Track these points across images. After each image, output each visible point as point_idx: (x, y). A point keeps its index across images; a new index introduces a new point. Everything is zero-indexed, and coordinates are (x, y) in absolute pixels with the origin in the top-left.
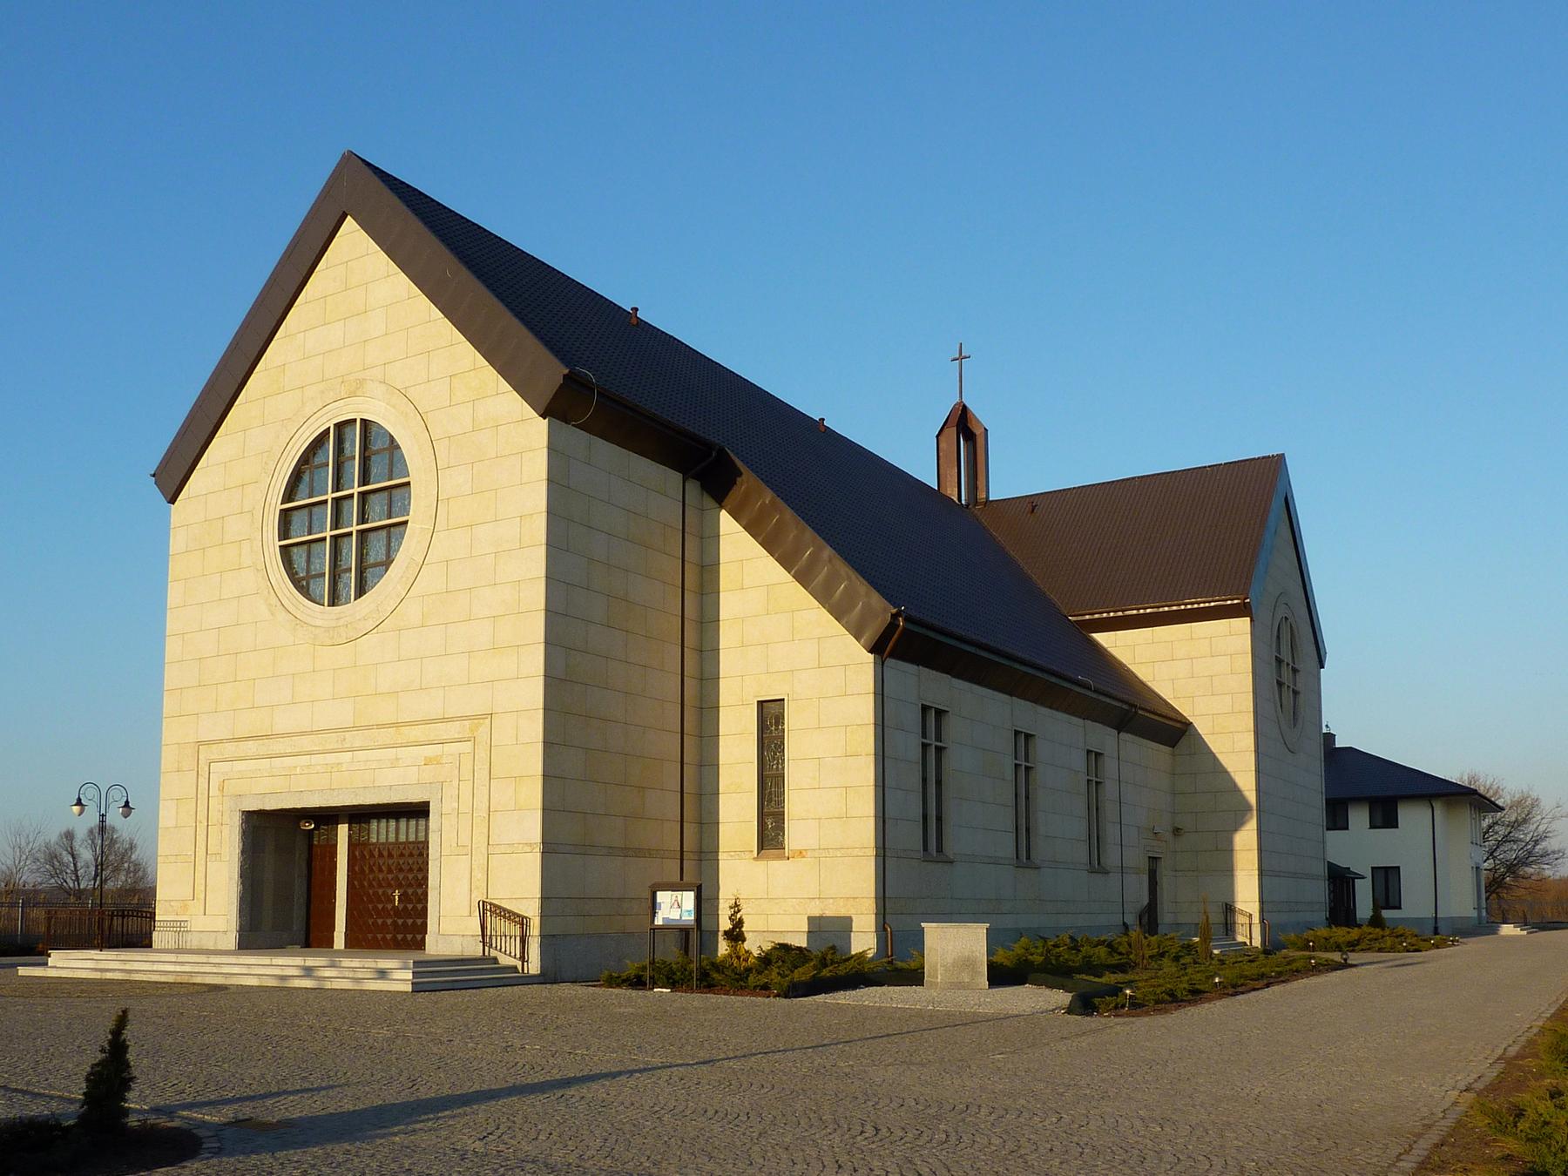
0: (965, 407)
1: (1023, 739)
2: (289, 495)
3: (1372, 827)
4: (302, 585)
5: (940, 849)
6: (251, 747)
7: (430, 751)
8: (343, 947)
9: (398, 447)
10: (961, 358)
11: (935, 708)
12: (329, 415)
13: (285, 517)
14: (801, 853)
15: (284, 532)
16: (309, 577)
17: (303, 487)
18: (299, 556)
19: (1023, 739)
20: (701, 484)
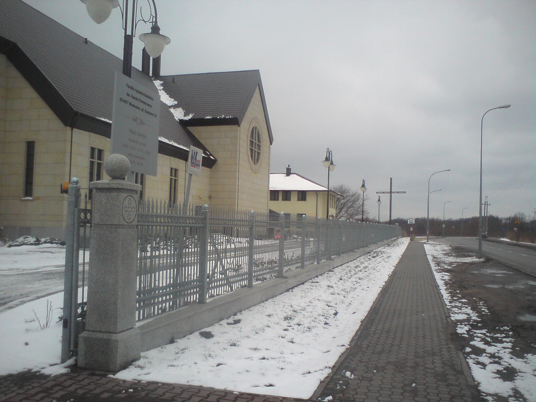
3: (298, 200)
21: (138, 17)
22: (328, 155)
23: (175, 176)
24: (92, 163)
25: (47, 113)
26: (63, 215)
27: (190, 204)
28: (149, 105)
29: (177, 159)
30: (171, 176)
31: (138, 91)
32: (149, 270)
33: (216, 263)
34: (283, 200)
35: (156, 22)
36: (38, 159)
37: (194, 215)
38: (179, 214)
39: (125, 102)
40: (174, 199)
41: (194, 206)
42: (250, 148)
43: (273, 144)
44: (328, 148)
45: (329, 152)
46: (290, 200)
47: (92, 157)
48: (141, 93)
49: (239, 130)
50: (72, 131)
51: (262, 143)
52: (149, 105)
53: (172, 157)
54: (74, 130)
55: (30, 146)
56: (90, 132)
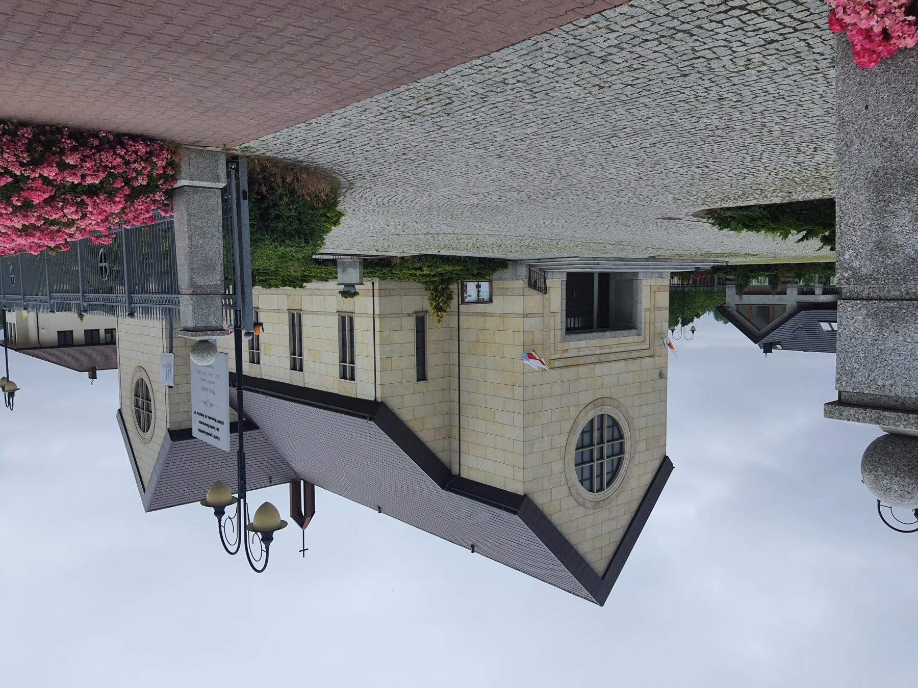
0: (302, 527)
1: (297, 365)
2: (620, 461)
3: (72, 332)
4: (615, 424)
5: (343, 319)
6: (634, 355)
7: (566, 355)
8: (833, 356)
9: (580, 481)
10: (304, 550)
11: (347, 379)
12: (606, 494)
13: (622, 452)
14: (409, 315)
15: (622, 444)
16: (612, 426)
17: (615, 464)
18: (616, 435)
19: (297, 365)
20: (451, 472)
21: (235, 520)
22: (11, 400)
23: (295, 359)
24: (352, 362)
25: (406, 415)
26: (194, 294)
28: (201, 423)
29: (253, 375)
30: (301, 360)
31: (211, 435)
34: (98, 330)
35: (220, 521)
39: (219, 422)
40: (294, 326)
42: (150, 401)
43: (117, 410)
44: (11, 410)
45: (9, 404)
46: (58, 332)
47: (353, 369)
48: (208, 434)
49: (168, 425)
50: (376, 397)
51: (134, 409)
52: (201, 423)
54: (373, 399)
55: (422, 376)
56: (305, 387)
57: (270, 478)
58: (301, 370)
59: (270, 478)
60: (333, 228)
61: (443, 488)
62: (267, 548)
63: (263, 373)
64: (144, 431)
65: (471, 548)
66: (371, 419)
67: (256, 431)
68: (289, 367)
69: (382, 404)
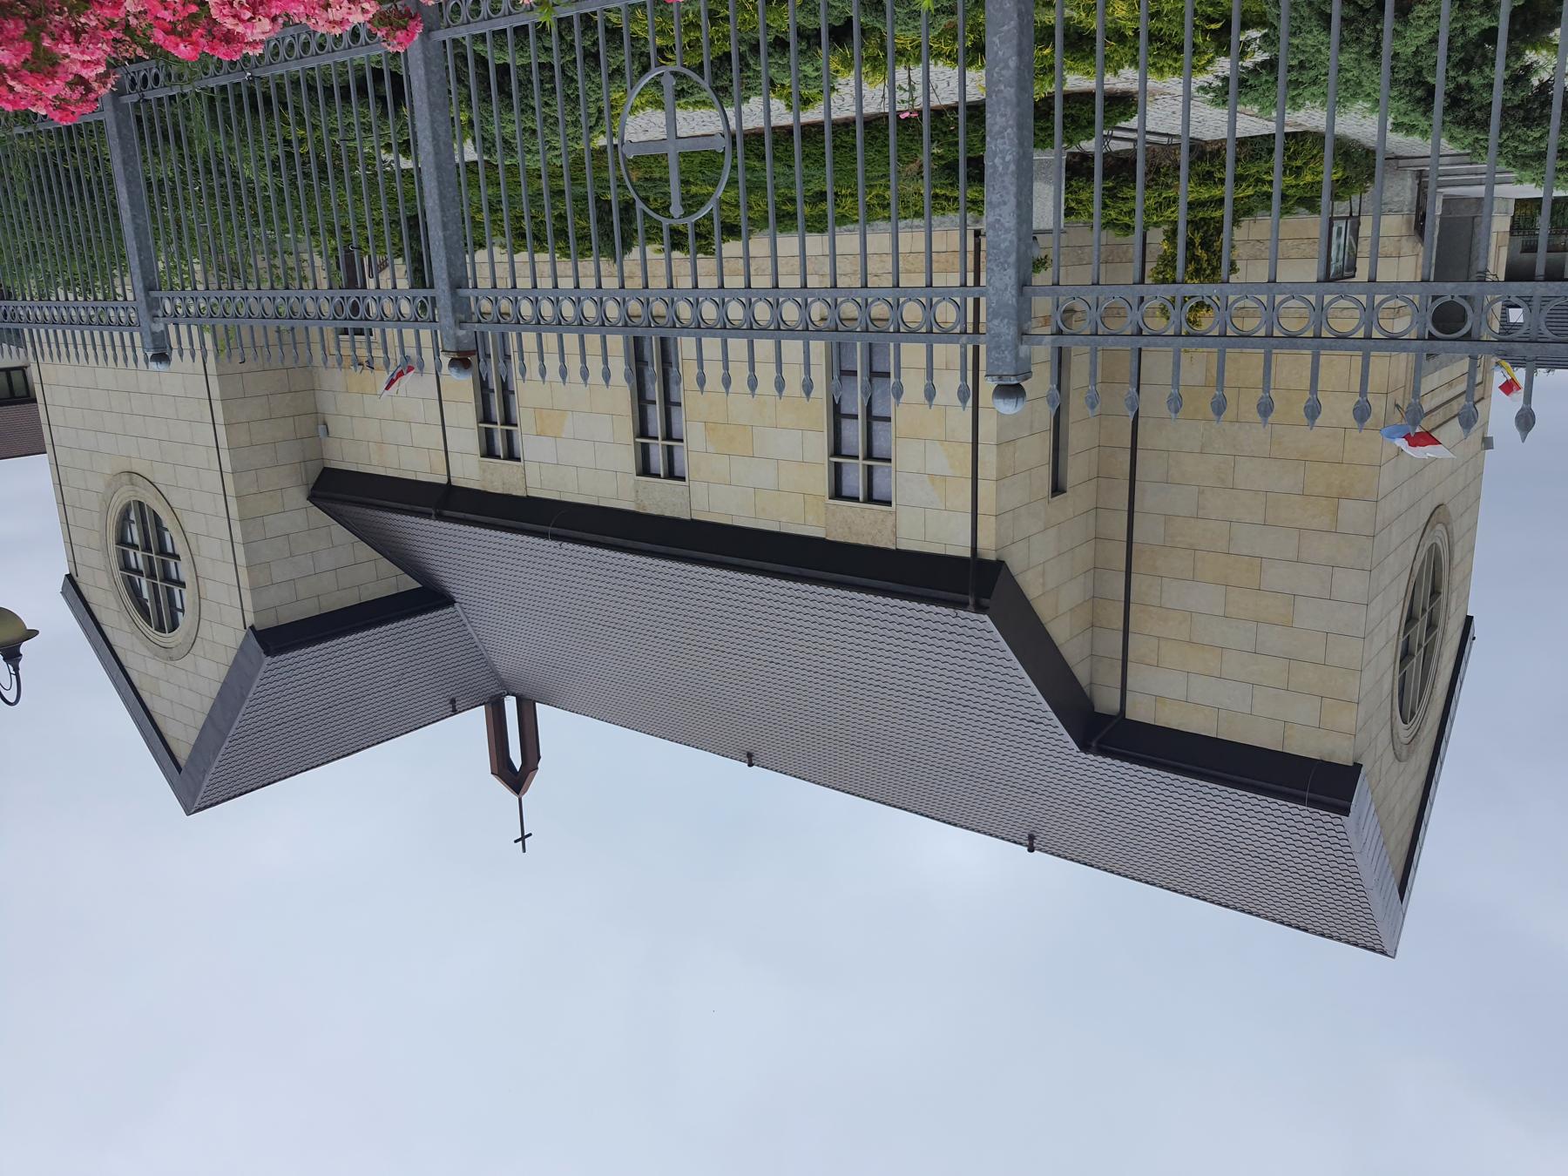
10: (523, 838)
11: (499, 457)
20: (1093, 708)
27: (193, 356)
32: (602, 175)
33: (673, 129)
36: (1045, 473)
37: (26, 331)
38: (436, 332)
41: (175, 355)
53: (520, 493)
56: (898, 551)
57: (453, 701)
58: (511, 455)
59: (453, 701)
60: (1127, 67)
61: (1084, 747)
62: (16, 669)
63: (901, 532)
64: (161, 628)
65: (1028, 842)
66: (980, 609)
67: (447, 611)
68: (634, 471)
69: (1000, 565)
